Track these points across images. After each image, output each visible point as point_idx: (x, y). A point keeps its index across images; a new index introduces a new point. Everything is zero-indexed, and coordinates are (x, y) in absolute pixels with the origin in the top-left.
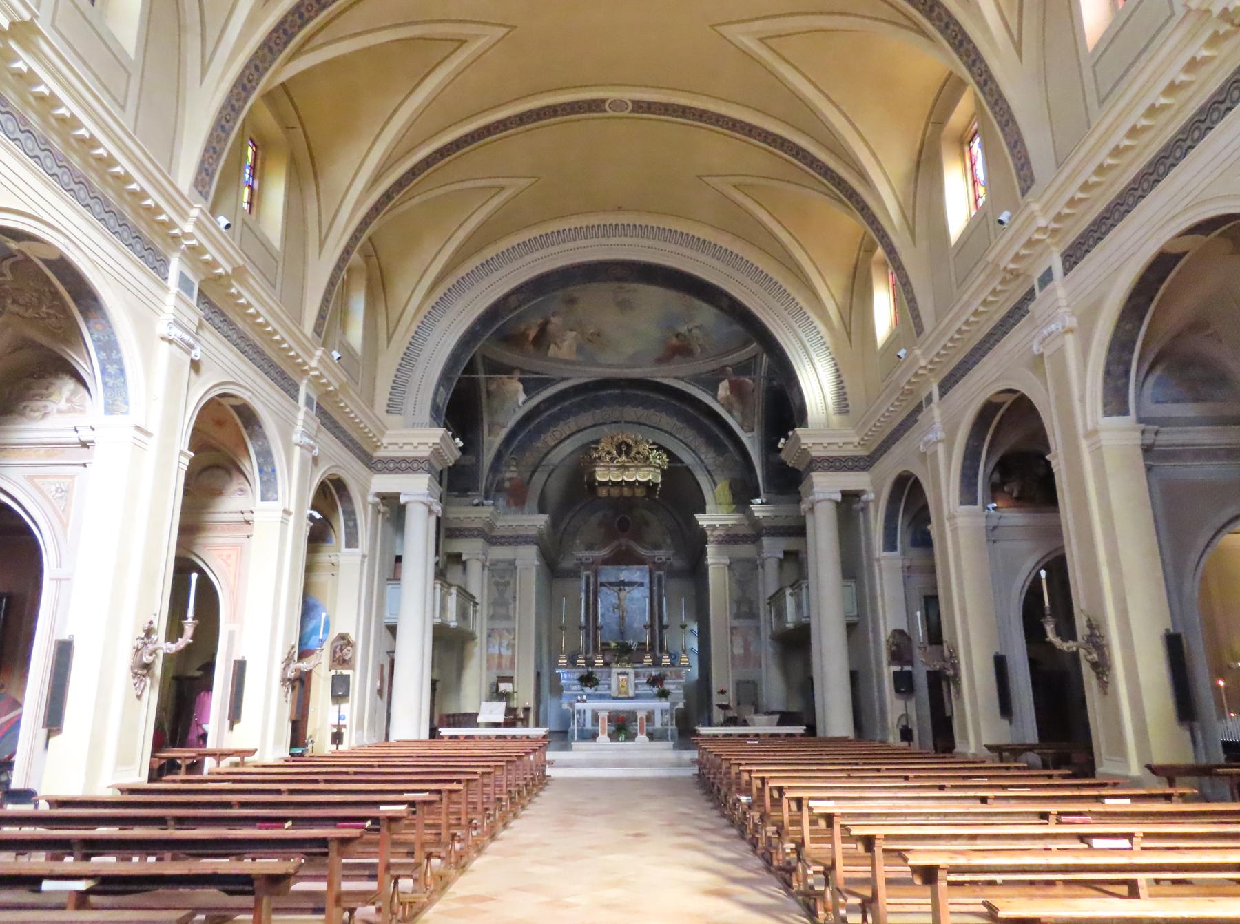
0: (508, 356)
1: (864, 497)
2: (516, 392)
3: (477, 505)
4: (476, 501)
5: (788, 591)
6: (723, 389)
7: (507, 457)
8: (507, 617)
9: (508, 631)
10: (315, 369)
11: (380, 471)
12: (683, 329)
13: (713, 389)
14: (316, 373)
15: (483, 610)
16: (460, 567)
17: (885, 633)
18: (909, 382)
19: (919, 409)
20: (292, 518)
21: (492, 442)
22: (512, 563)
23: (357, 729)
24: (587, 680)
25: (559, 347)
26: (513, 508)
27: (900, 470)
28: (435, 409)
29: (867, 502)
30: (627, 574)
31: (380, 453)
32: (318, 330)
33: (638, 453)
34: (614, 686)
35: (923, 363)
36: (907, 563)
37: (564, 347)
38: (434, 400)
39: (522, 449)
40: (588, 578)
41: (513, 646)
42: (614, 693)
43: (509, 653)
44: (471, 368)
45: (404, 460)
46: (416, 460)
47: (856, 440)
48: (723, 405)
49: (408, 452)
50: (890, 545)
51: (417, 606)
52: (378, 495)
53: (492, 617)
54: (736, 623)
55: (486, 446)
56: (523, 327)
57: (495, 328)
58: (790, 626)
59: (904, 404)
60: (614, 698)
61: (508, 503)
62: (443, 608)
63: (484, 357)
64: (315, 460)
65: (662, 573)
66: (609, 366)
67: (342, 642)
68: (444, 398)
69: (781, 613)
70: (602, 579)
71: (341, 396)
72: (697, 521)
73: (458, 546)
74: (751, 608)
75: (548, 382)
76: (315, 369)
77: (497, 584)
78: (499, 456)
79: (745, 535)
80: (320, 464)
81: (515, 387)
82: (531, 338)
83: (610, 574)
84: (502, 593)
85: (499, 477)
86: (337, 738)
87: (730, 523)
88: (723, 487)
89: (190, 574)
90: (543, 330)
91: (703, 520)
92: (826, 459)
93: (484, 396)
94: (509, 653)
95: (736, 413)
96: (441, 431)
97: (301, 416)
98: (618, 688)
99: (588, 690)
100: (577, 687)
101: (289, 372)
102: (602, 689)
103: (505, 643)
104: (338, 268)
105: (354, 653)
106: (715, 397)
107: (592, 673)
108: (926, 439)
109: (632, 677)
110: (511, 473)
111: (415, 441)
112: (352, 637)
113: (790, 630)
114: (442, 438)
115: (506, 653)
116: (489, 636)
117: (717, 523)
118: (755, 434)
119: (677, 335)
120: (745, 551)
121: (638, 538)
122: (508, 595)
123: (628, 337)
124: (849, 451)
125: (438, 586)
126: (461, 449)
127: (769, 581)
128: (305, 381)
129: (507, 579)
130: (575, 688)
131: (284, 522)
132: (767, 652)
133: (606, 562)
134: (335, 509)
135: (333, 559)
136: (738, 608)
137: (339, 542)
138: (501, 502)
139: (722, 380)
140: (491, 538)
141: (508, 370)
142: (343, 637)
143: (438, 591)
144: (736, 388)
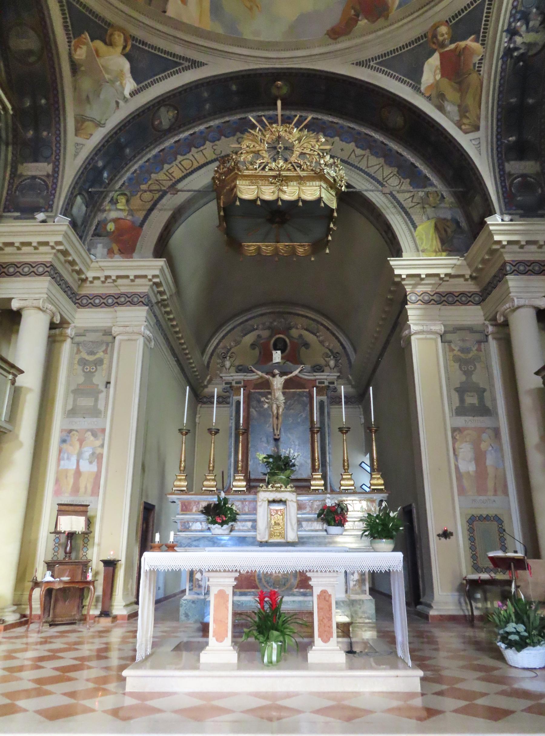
2: (120, 75)
6: (431, 70)
8: (95, 412)
9: (94, 434)
22: (107, 332)
24: (218, 513)
34: (262, 524)
41: (99, 457)
42: (262, 534)
43: (94, 468)
48: (429, 98)
54: (461, 421)
60: (262, 544)
61: (111, 252)
72: (392, 270)
74: (481, 399)
75: (167, 64)
77: (83, 362)
81: (117, 62)
84: (89, 375)
85: (101, 216)
87: (442, 272)
88: (425, 229)
91: (401, 267)
94: (94, 468)
95: (449, 108)
98: (269, 526)
99: (217, 529)
102: (242, 527)
103: (87, 452)
106: (417, 89)
107: (226, 500)
109: (292, 507)
113: (476, 472)
114: (88, 267)
115: (87, 468)
116: (64, 441)
117: (423, 272)
118: (481, 134)
122: (98, 380)
129: (100, 355)
130: (197, 526)
136: (462, 400)
139: (430, 54)
144: (455, 69)
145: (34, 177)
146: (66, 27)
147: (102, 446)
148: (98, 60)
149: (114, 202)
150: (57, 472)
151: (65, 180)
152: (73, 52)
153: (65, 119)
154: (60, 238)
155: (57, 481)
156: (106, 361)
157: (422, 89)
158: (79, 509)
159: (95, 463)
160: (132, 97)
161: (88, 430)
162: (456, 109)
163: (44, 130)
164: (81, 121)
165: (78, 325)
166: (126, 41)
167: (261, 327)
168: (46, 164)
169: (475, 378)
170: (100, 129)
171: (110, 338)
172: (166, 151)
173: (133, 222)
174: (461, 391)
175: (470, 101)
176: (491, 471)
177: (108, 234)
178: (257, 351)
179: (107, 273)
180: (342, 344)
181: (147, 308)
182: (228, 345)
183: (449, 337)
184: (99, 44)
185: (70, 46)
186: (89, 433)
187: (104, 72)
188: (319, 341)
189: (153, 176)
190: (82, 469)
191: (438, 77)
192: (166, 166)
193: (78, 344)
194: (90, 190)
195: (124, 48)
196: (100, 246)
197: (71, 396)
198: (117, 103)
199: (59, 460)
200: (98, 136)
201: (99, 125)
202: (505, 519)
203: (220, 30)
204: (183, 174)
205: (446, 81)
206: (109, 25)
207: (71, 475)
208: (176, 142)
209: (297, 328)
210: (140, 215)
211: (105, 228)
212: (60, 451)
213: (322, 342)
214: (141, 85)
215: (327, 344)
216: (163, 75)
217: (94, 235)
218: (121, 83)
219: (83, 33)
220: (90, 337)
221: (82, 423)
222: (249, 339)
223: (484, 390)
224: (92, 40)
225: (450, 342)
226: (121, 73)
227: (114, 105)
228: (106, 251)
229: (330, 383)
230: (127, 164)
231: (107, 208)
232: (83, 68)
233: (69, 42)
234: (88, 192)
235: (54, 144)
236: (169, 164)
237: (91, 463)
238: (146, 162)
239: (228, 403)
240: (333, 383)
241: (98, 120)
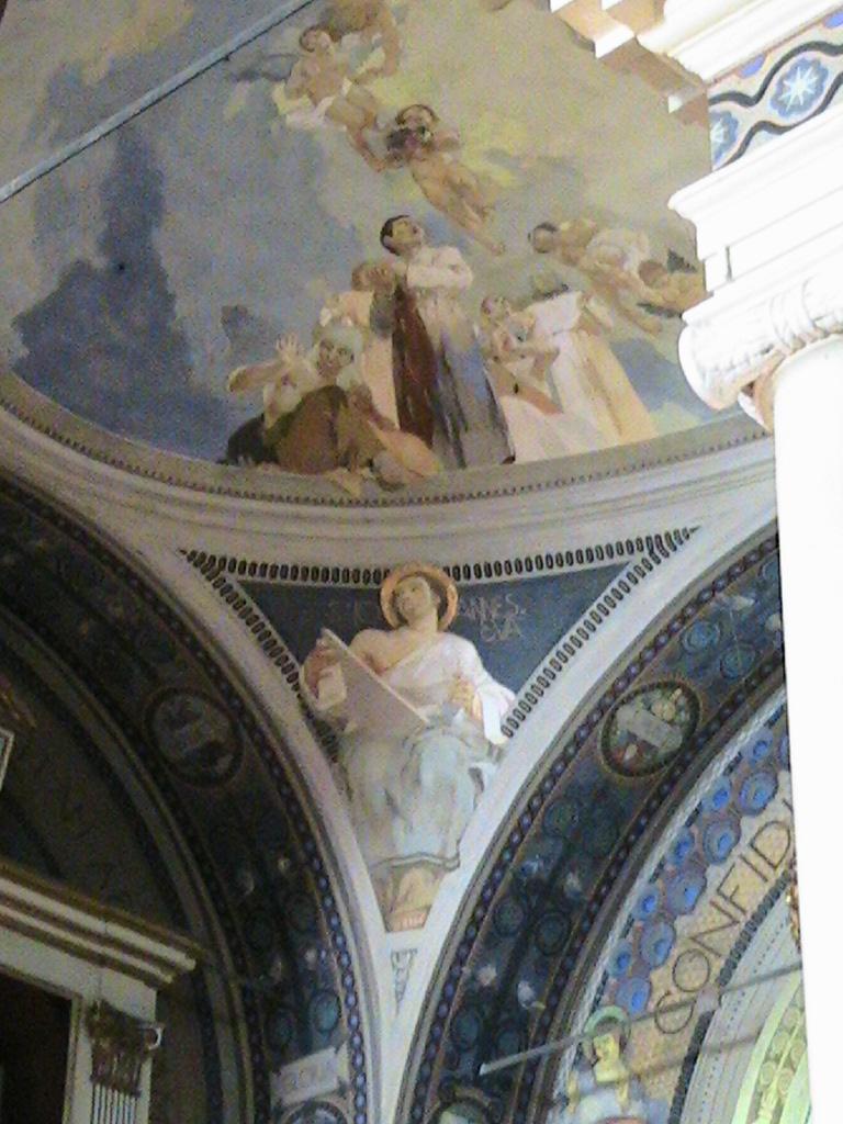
25: (552, 406)
55: (384, 980)
79: (730, 976)
81: (438, 662)
82: (386, 402)
89: (277, 864)
93: (304, 745)
146: (269, 648)
148: (380, 680)
149: (586, 1062)
151: (384, 1092)
152: (310, 698)
160: (511, 735)
163: (308, 946)
164: (389, 876)
166: (438, 589)
168: (332, 1050)
170: (450, 877)
172: (705, 815)
184: (369, 639)
185: (297, 688)
187: (410, 706)
192: (714, 873)
194: (484, 1070)
195: (442, 609)
198: (476, 775)
200: (446, 903)
201: (443, 865)
204: (767, 888)
208: (730, 769)
210: (663, 1088)
214: (527, 688)
216: (580, 624)
218: (469, 711)
219: (319, 635)
224: (348, 640)
226: (459, 681)
227: (466, 784)
230: (592, 918)
231: (571, 1089)
232: (351, 727)
233: (293, 679)
234: (478, 1081)
235: (339, 980)
238: (656, 875)
241: (436, 851)
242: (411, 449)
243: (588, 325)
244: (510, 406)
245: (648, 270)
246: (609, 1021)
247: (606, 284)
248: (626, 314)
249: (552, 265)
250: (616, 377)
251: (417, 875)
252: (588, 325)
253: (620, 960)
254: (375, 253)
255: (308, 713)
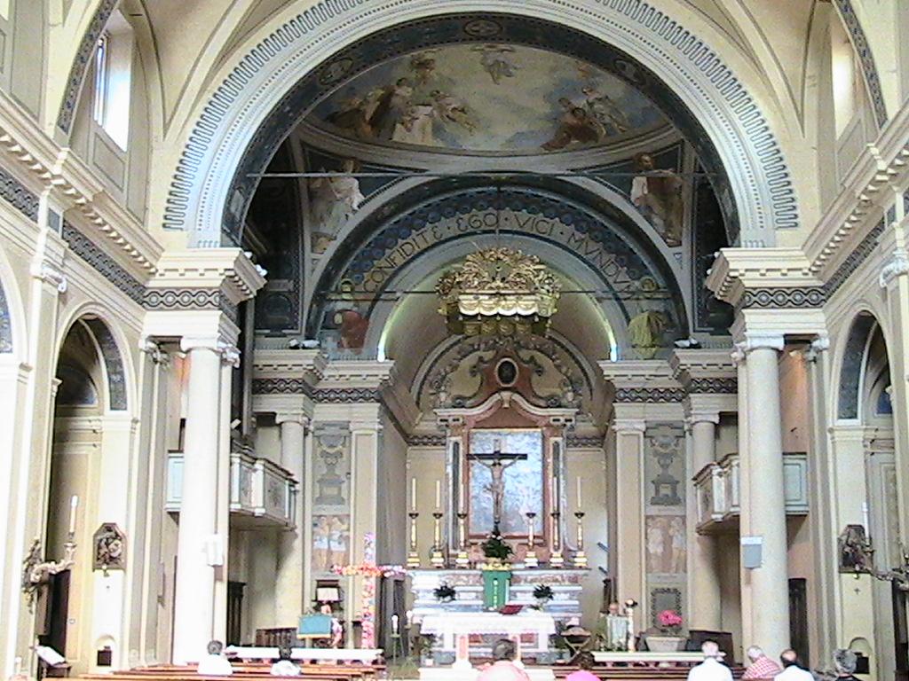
0: (330, 143)
1: (815, 344)
3: (296, 347)
4: (293, 343)
5: (716, 470)
6: (639, 186)
7: (338, 281)
10: (60, 176)
11: (153, 306)
12: (581, 103)
13: (625, 187)
14: (61, 182)
15: (308, 489)
16: (275, 431)
17: (838, 528)
18: (866, 191)
19: (879, 228)
20: (32, 375)
21: (315, 261)
22: (345, 426)
23: (131, 647)
25: (409, 130)
26: (347, 351)
27: (859, 308)
28: (229, 223)
29: (819, 351)
30: (515, 441)
31: (153, 283)
32: (62, 125)
33: (519, 275)
35: (882, 165)
36: (871, 434)
37: (416, 130)
38: (227, 209)
39: (358, 269)
40: (456, 444)
43: (343, 548)
44: (283, 160)
45: (186, 291)
46: (202, 291)
47: (807, 264)
49: (192, 281)
50: (849, 411)
51: (206, 485)
52: (153, 338)
53: (319, 500)
54: (654, 510)
56: (357, 101)
57: (314, 105)
58: (719, 517)
59: (863, 219)
61: (340, 345)
62: (245, 490)
63: (303, 144)
64: (63, 297)
65: (559, 439)
66: (478, 155)
67: (108, 534)
68: (241, 205)
69: (707, 500)
70: (476, 449)
71: (96, 210)
73: (268, 403)
74: (674, 490)
76: (60, 176)
77: (325, 454)
78: (326, 279)
80: (70, 303)
81: (348, 184)
82: (368, 118)
83: (485, 442)
84: (331, 466)
85: (328, 307)
86: (104, 658)
90: (385, 101)
92: (763, 291)
95: (656, 220)
96: (236, 251)
97: (41, 239)
100: (431, 598)
101: (26, 183)
103: (336, 536)
104: (90, 38)
105: (125, 549)
106: (627, 197)
108: (885, 269)
110: (341, 304)
111: (201, 266)
112: (121, 529)
115: (335, 546)
116: (315, 525)
119: (574, 111)
120: (669, 412)
121: (526, 391)
122: (339, 471)
123: (497, 122)
124: (796, 280)
125: (236, 461)
126: (266, 277)
127: (699, 450)
128: (46, 193)
131: (21, 381)
132: (694, 549)
133: (481, 424)
134: (95, 357)
135: (95, 425)
136: (657, 491)
137: (101, 404)
138: (330, 343)
140: (312, 390)
141: (335, 163)
142: (108, 528)
143: (236, 467)
144: (659, 188)
145: (279, 293)
147: (348, 530)
150: (312, 551)
153: (302, 236)
154: (311, 362)
155: (313, 558)
156: (345, 454)
157: (633, 199)
158: (333, 584)
159: (343, 544)
161: (334, 516)
162: (662, 222)
164: (316, 237)
165: (319, 420)
167: (482, 346)
169: (671, 471)
171: (345, 432)
173: (360, 315)
174: (657, 484)
175: (673, 218)
176: (675, 552)
177: (336, 327)
178: (479, 377)
179: (341, 373)
180: (583, 370)
181: (379, 404)
182: (442, 370)
183: (650, 433)
186: (336, 519)
188: (556, 366)
189: (375, 262)
190: (333, 549)
191: (646, 192)
192: (388, 251)
193: (319, 437)
196: (330, 339)
197: (318, 485)
199: (313, 541)
202: (683, 591)
203: (441, 144)
205: (651, 196)
206: (341, 157)
207: (324, 553)
209: (528, 349)
210: (366, 306)
211: (333, 320)
212: (313, 533)
213: (558, 367)
215: (564, 370)
217: (323, 328)
220: (330, 431)
221: (329, 510)
222: (470, 360)
223: (678, 482)
225: (651, 437)
227: (344, 217)
228: (336, 344)
229: (567, 420)
236: (391, 248)
237: (340, 543)
239: (444, 445)
240: (571, 420)
242: (368, 129)
243: (431, 115)
244: (398, 126)
245: (454, 109)
246: (347, 283)
247: (441, 109)
248: (442, 117)
249: (432, 100)
250: (429, 129)
251: (323, 239)
252: (431, 115)
253: (353, 266)
254: (394, 84)
255: (308, 187)
